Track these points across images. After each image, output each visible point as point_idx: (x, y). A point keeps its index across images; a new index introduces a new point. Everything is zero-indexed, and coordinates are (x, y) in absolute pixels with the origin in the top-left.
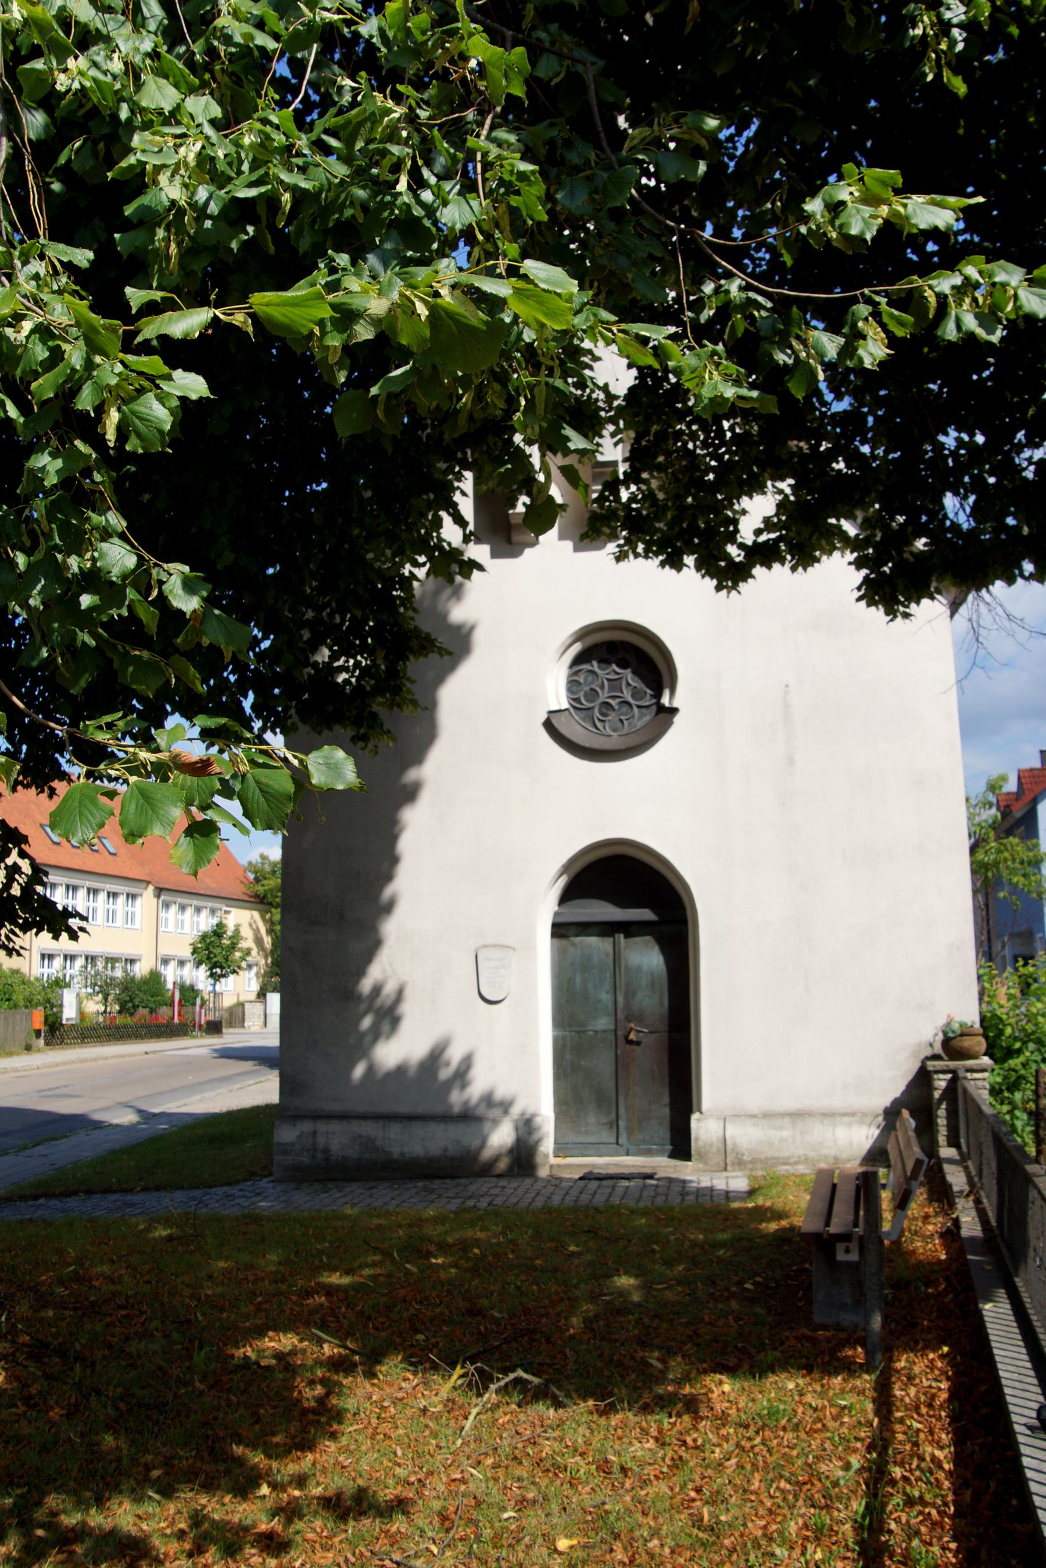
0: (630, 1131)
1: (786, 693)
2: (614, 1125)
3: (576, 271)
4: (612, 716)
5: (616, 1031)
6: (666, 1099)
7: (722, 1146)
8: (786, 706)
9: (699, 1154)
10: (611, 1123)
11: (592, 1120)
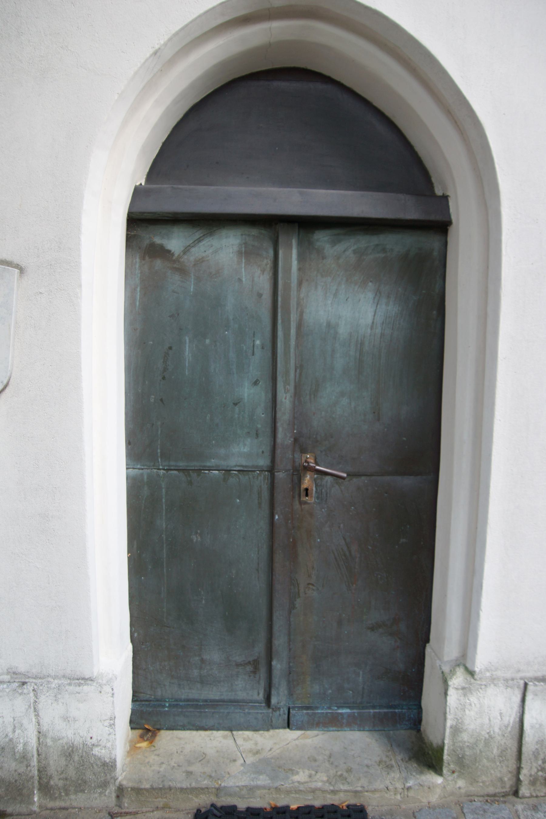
0: (293, 678)
2: (262, 666)
5: (272, 470)
7: (513, 745)
9: (460, 761)
10: (255, 664)
11: (214, 655)
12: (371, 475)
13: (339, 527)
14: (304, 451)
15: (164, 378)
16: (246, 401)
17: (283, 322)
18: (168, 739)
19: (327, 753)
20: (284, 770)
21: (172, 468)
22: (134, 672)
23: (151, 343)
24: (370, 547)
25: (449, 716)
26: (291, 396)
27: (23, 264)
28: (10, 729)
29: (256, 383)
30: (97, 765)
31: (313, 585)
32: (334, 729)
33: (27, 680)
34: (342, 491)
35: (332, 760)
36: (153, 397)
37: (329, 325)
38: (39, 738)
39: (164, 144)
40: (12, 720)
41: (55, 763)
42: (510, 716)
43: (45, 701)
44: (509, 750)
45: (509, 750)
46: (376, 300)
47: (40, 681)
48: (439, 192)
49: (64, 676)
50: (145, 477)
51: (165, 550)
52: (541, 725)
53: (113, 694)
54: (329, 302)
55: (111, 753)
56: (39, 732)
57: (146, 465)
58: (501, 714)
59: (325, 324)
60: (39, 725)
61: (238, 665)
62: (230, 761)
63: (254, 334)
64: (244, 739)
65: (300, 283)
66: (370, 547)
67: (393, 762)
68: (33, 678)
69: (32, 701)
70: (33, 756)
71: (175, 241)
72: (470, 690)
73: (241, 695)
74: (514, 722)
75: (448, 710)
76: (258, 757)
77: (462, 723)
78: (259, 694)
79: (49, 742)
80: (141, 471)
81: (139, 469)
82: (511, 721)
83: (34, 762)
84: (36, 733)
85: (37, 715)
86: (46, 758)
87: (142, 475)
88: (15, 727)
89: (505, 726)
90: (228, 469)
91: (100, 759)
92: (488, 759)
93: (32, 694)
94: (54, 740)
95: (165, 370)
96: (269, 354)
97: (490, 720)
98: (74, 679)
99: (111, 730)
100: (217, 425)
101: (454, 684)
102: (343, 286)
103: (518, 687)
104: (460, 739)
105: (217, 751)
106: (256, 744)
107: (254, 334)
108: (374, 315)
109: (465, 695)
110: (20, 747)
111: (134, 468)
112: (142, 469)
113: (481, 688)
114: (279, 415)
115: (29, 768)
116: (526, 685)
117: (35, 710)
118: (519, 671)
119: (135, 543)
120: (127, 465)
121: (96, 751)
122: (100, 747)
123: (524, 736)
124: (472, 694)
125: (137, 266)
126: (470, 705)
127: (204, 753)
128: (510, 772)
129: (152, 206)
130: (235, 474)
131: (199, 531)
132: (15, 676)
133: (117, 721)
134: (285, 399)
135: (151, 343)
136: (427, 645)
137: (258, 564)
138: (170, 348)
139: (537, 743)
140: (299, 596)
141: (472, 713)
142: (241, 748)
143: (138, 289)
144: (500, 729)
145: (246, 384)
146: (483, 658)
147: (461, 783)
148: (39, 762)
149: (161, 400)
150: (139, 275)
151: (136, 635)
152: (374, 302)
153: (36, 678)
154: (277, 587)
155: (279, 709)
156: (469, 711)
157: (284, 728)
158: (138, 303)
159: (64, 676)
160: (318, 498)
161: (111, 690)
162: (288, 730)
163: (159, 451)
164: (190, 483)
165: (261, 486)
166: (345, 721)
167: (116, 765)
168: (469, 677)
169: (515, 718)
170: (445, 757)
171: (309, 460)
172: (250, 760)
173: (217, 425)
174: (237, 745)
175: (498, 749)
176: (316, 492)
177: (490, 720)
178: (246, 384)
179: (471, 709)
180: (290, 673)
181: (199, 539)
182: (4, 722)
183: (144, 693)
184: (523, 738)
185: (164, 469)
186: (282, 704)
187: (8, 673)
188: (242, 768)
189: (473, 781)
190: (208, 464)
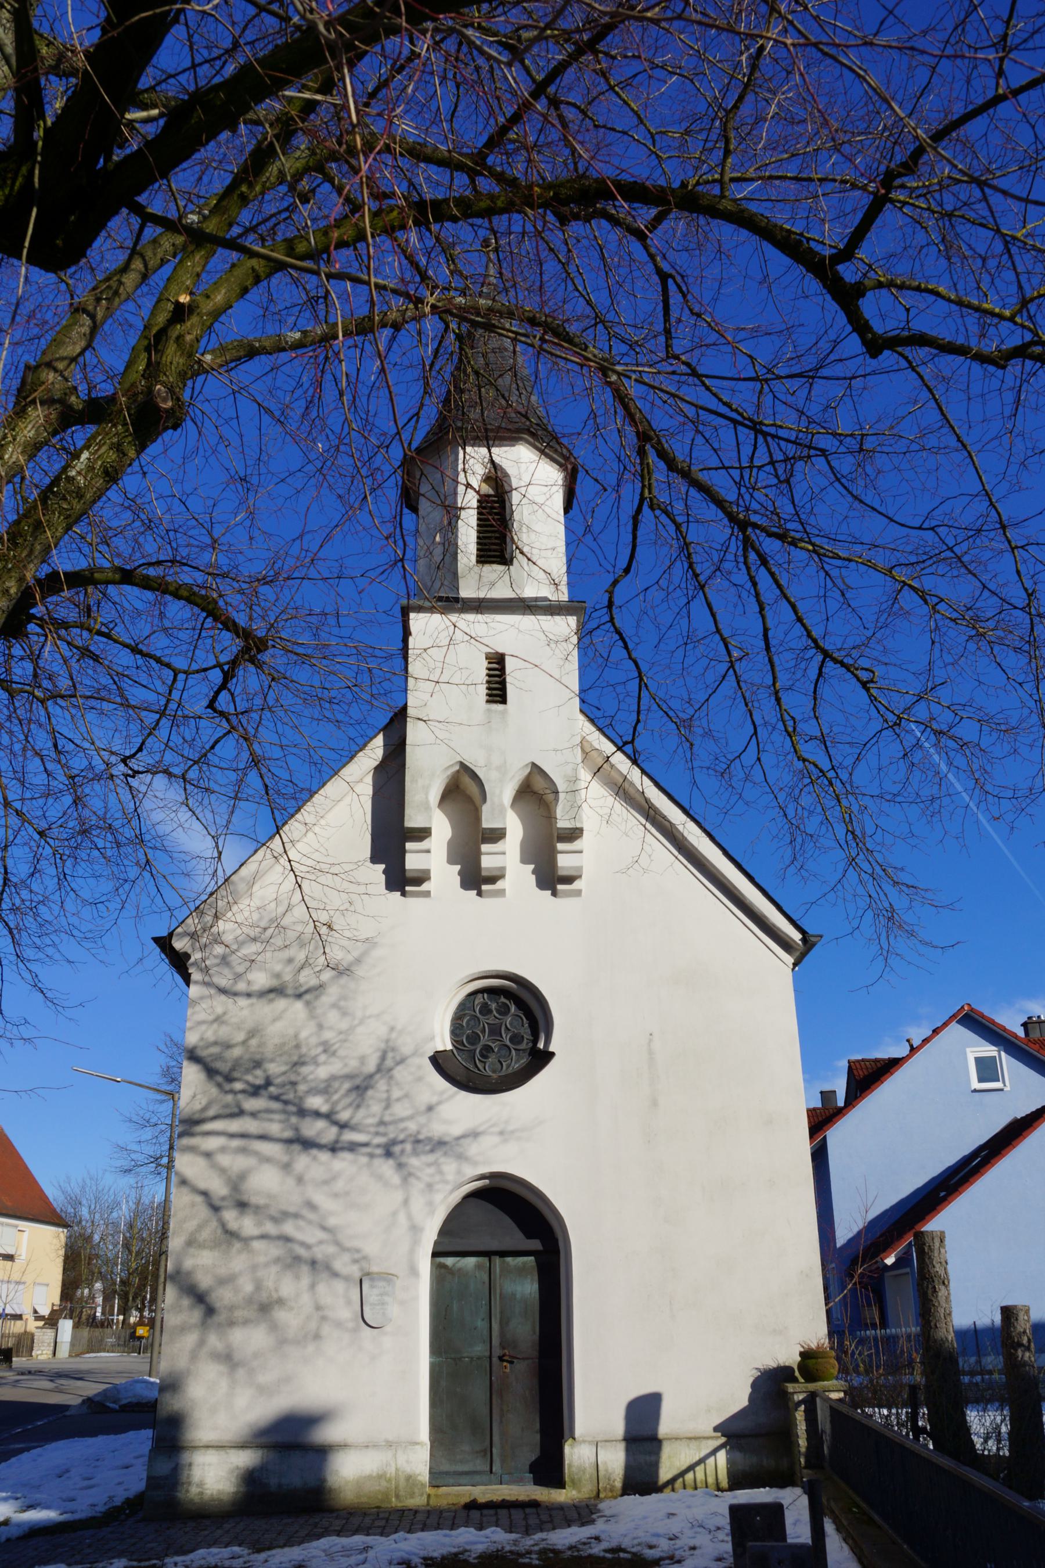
1: (650, 1041)
2: (488, 1453)
4: (492, 1059)
8: (651, 1052)
9: (573, 1481)
11: (466, 1448)
41: (402, 1483)
43: (400, 1453)
71: (449, 1261)
73: (479, 1468)
129: (441, 1249)
146: (579, 1431)
147: (574, 1492)
189: (579, 1492)
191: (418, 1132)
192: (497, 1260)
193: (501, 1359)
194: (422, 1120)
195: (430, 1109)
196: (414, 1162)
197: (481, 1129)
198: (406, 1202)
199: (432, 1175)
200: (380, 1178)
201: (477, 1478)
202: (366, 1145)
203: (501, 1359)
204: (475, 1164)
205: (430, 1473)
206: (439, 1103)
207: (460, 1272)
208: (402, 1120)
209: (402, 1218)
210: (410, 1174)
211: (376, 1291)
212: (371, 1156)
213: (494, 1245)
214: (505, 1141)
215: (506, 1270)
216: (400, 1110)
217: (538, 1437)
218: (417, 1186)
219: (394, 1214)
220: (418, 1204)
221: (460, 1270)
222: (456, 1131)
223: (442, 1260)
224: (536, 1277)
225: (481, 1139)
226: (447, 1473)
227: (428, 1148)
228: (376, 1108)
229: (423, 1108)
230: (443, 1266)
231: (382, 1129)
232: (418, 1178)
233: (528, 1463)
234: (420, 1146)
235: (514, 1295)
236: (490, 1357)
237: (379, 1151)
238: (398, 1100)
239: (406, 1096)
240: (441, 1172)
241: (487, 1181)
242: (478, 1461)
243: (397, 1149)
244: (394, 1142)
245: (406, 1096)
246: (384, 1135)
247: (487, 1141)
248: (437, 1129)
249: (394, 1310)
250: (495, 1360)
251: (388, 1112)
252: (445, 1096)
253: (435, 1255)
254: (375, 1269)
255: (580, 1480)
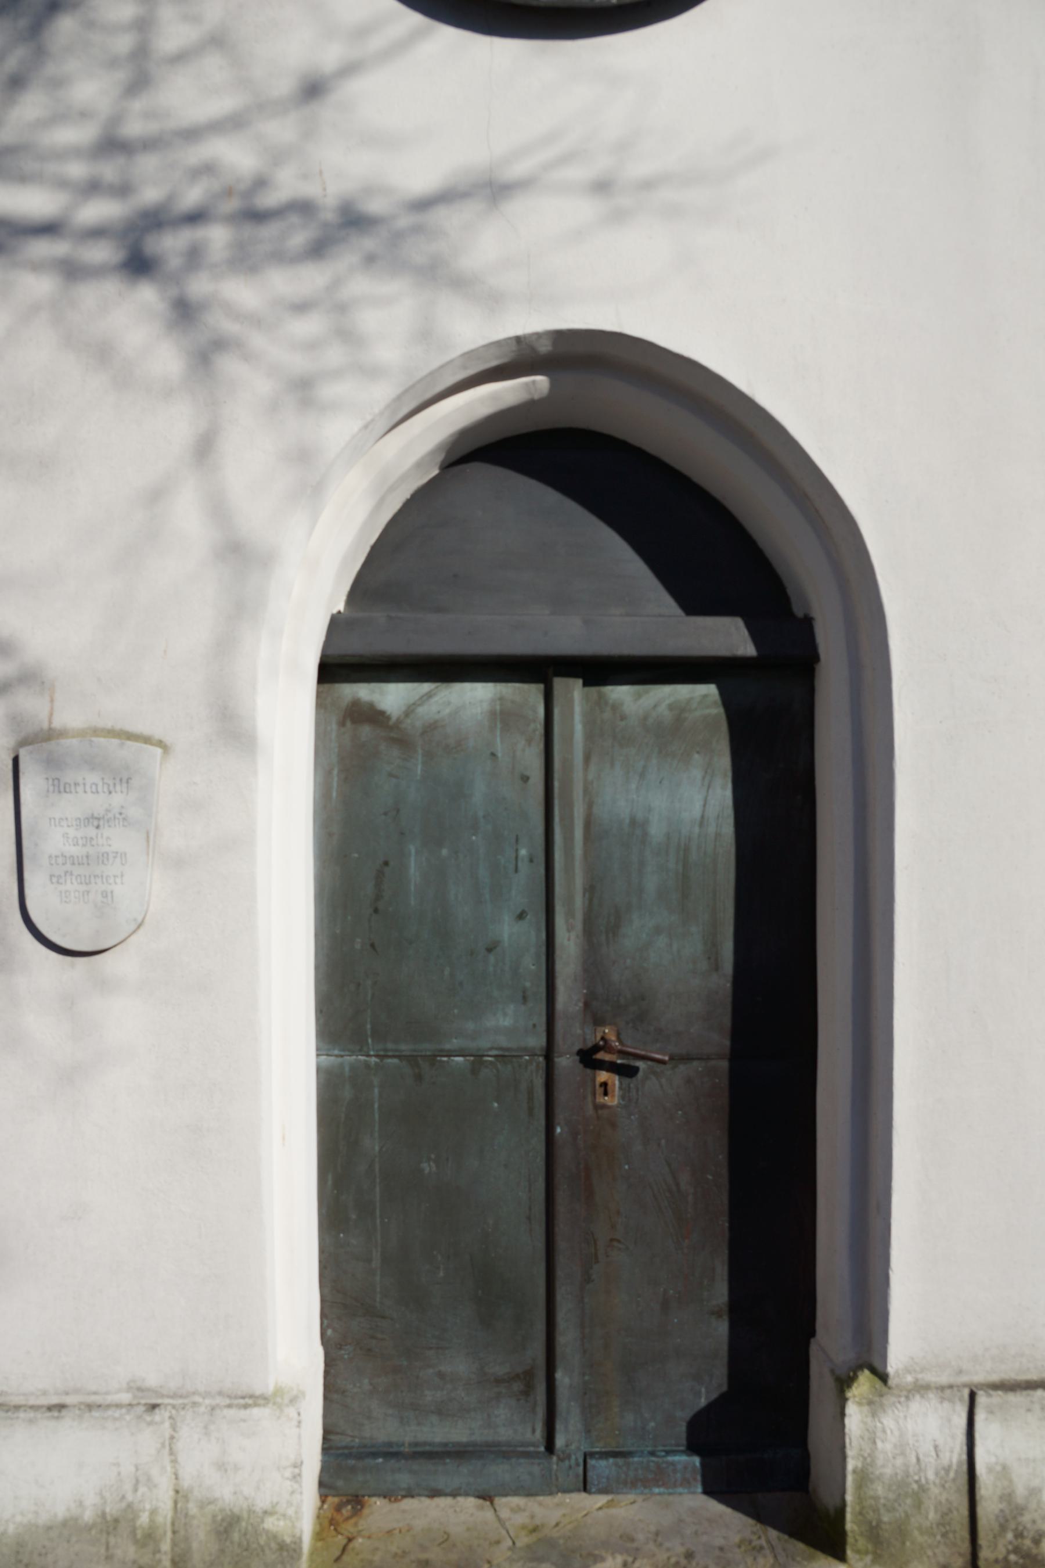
2: (539, 1385)
3: (380, 1150)
5: (549, 1053)
6: (720, 1293)
9: (874, 1533)
11: (460, 1366)
12: (708, 1058)
13: (659, 1145)
14: (598, 1021)
15: (376, 911)
16: (506, 945)
17: (562, 819)
18: (380, 1512)
19: (653, 1528)
20: (581, 1556)
21: (390, 1053)
22: (326, 1398)
23: (356, 855)
24: (710, 1177)
25: (850, 1452)
26: (577, 936)
27: (168, 740)
28: (128, 1487)
29: (521, 916)
30: (270, 1549)
31: (619, 1241)
32: (662, 1490)
33: (159, 1401)
34: (661, 1086)
35: (660, 1539)
36: (359, 940)
37: (633, 822)
38: (176, 1503)
39: (374, 548)
40: (133, 1469)
42: (952, 1451)
43: (189, 1434)
44: (955, 1513)
45: (955, 1513)
46: (706, 782)
47: (180, 1401)
48: (799, 613)
49: (220, 1393)
50: (347, 1069)
51: (378, 1189)
52: (1005, 1467)
53: (299, 1422)
54: (633, 786)
55: (294, 1527)
56: (177, 1492)
57: (349, 1050)
58: (936, 1447)
59: (627, 821)
60: (177, 1478)
61: (498, 1381)
62: (490, 1544)
63: (517, 840)
64: (512, 1510)
65: (587, 759)
66: (710, 1177)
67: (763, 1542)
68: (169, 1397)
69: (167, 1436)
70: (165, 1533)
71: (392, 696)
72: (882, 1405)
73: (504, 1434)
74: (959, 1463)
75: (847, 1441)
76: (534, 1537)
77: (873, 1464)
78: (534, 1431)
79: (193, 1509)
80: (340, 1060)
81: (336, 1056)
82: (955, 1460)
83: (166, 1546)
84: (171, 1493)
85: (174, 1462)
86: (187, 1539)
87: (341, 1066)
88: (137, 1481)
89: (944, 1468)
90: (480, 1053)
91: (275, 1537)
92: (920, 1529)
93: (167, 1424)
94: (202, 1505)
95: (378, 897)
96: (542, 870)
97: (918, 1459)
98: (236, 1397)
99: (296, 1486)
100: (461, 984)
101: (854, 1396)
102: (654, 761)
103: (961, 1400)
104: (871, 1493)
105: (468, 1529)
106: (532, 1517)
107: (517, 840)
108: (704, 806)
109: (874, 1415)
110: (144, 1519)
111: (328, 1055)
112: (342, 1056)
113: (899, 1402)
114: (559, 966)
115: (158, 1556)
116: (972, 1396)
117: (171, 1452)
118: (960, 1372)
119: (330, 1177)
120: (317, 1049)
121: (271, 1524)
122: (275, 1517)
123: (977, 1486)
124: (884, 1411)
125: (334, 735)
126: (884, 1431)
127: (445, 1533)
128: (960, 1554)
129: (357, 646)
130: (491, 1062)
131: (433, 1156)
132: (140, 1394)
133: (304, 1468)
134: (569, 940)
135: (356, 855)
136: (812, 1340)
137: (530, 1209)
138: (386, 863)
139: (1001, 1498)
140: (597, 1262)
141: (888, 1447)
142: (507, 1524)
143: (335, 772)
144: (937, 1474)
145: (506, 918)
146: (901, 1349)
148: (174, 1544)
149: (373, 946)
150: (336, 750)
151: (329, 1332)
152: (703, 785)
153: (174, 1396)
154: (561, 1244)
155: (569, 1457)
156: (883, 1441)
157: (579, 1490)
158: (334, 794)
159: (220, 1393)
160: (623, 1097)
161: (296, 1415)
162: (584, 1495)
163: (369, 1026)
164: (419, 1078)
165: (532, 1081)
166: (679, 1475)
167: (301, 1548)
168: (878, 1384)
169: (960, 1455)
170: (849, 1526)
171: (607, 1037)
172: (523, 1540)
173: (461, 984)
174: (498, 1517)
175: (936, 1511)
176: (620, 1088)
177: (918, 1459)
178: (506, 918)
179: (889, 1440)
180: (585, 1394)
181: (434, 1169)
182: (119, 1474)
183: (342, 1434)
184: (977, 1490)
185: (376, 1056)
186: (573, 1447)
187: (129, 1389)
188: (509, 1553)
190: (447, 1046)
191: (261, 183)
192: (573, 693)
193: (588, 1058)
194: (281, 130)
195: (313, 89)
196: (242, 293)
197: (519, 170)
198: (204, 448)
199: (312, 346)
200: (102, 353)
201: (500, 1471)
202: (49, 229)
203: (588, 1058)
204: (494, 301)
205: (328, 1447)
206: (350, 69)
207: (434, 740)
208: (192, 134)
209: (187, 514)
210: (220, 344)
211: (70, 806)
212: (72, 271)
213: (568, 635)
214: (618, 217)
215: (606, 736)
216: (188, 97)
217: (722, 1328)
218: (249, 384)
219: (156, 496)
220: (250, 456)
221: (432, 727)
222: (418, 174)
223: (364, 692)
224: (724, 761)
225: (516, 207)
226: (391, 1453)
227: (299, 239)
228: (92, 89)
229: (284, 86)
230: (373, 716)
231: (109, 171)
232: (248, 356)
233: (683, 1416)
234: (269, 231)
235: (638, 826)
236: (549, 1053)
237: (101, 253)
238: (180, 58)
239: (217, 41)
240: (347, 335)
241: (541, 382)
242: (502, 1412)
243: (170, 245)
244: (155, 220)
245: (217, 41)
246: (123, 190)
247: (542, 219)
248: (336, 166)
249: (143, 887)
250: (566, 1062)
251: (137, 105)
252: (376, 42)
253: (331, 671)
254: (70, 716)
255: (902, 1531)
